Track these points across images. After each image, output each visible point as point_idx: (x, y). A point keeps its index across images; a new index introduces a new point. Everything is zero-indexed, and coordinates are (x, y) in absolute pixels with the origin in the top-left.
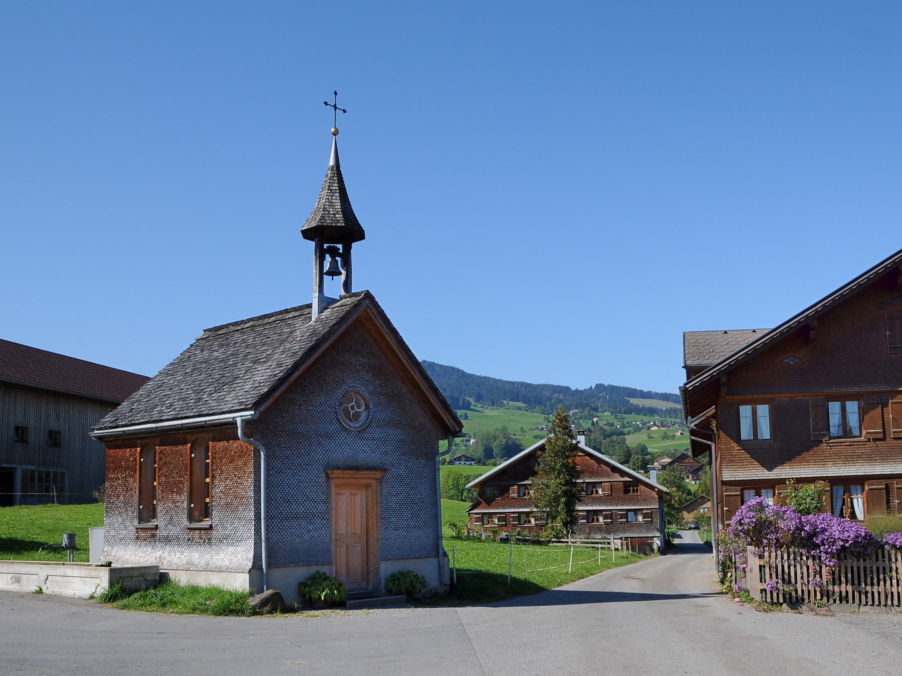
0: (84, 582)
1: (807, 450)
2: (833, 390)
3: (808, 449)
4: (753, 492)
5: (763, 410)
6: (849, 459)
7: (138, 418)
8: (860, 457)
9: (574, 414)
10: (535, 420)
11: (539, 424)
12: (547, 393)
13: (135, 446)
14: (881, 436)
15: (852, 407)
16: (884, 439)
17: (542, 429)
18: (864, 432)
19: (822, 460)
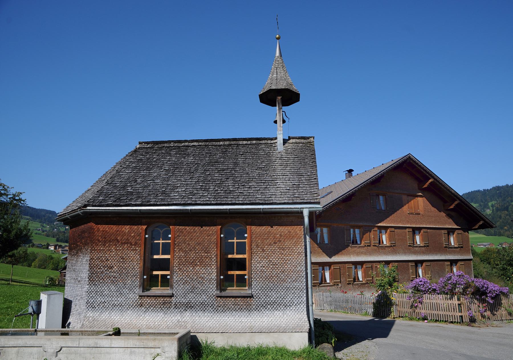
0: (131, 353)
1: (344, 250)
2: (353, 223)
3: (344, 249)
4: (328, 267)
5: (325, 230)
6: (358, 254)
7: (274, 199)
8: (362, 253)
9: (56, 224)
10: (36, 226)
11: (38, 227)
12: (43, 213)
13: (141, 224)
14: (369, 244)
15: (357, 231)
16: (370, 246)
17: (39, 230)
18: (363, 242)
19: (349, 254)
